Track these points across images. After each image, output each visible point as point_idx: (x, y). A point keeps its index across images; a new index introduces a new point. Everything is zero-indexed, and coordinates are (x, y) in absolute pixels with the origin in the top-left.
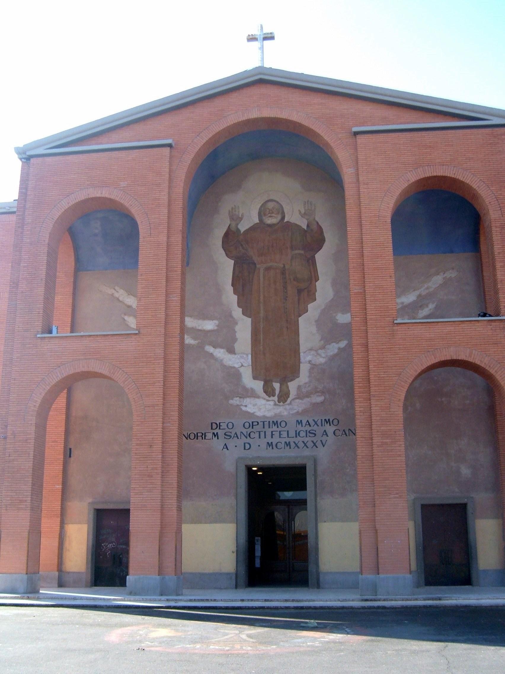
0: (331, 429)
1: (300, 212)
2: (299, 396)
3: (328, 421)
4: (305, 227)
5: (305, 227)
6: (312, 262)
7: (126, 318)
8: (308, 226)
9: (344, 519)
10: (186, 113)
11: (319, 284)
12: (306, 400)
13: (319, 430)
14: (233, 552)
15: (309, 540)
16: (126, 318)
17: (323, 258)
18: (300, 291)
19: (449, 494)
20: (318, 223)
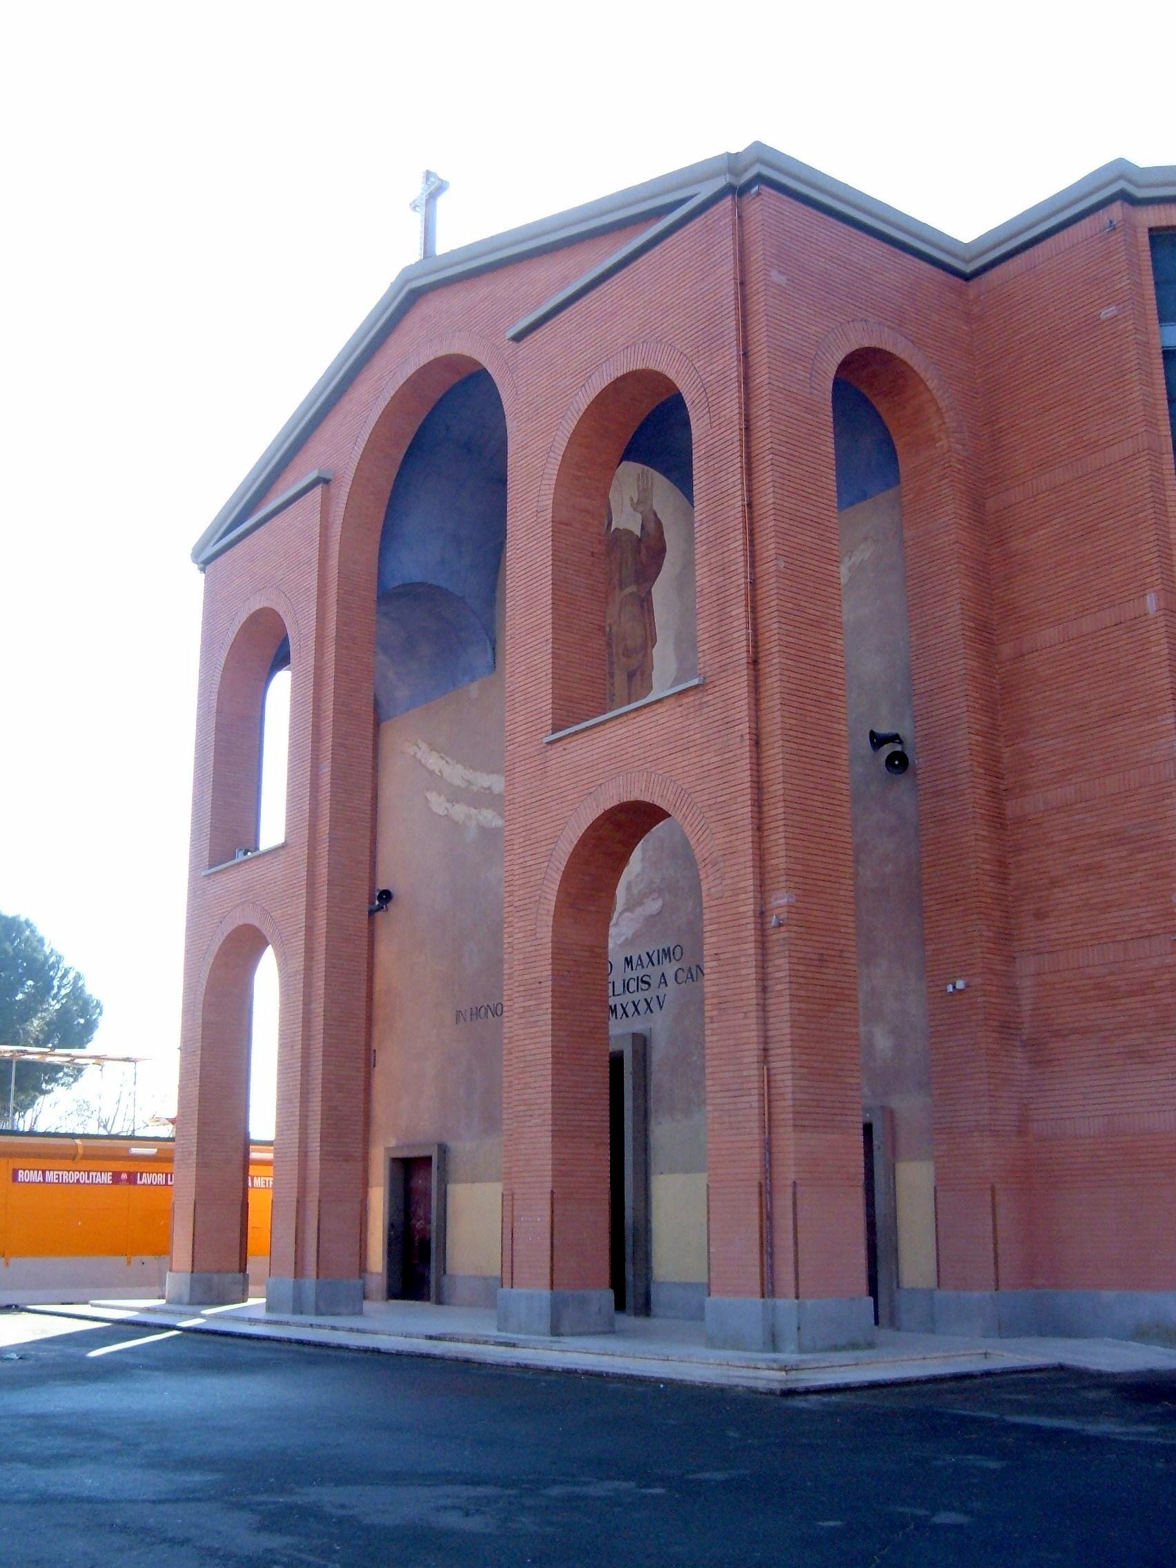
0: (670, 968)
1: (632, 499)
2: (628, 909)
3: (667, 953)
4: (638, 532)
5: (638, 532)
6: (645, 603)
7: (428, 795)
8: (643, 528)
9: (688, 1169)
10: (482, 289)
11: (656, 651)
12: (639, 910)
13: (654, 973)
14: (414, 207)
15: (632, 1317)
16: (428, 795)
17: (661, 591)
18: (631, 676)
19: (867, 1121)
20: (655, 515)
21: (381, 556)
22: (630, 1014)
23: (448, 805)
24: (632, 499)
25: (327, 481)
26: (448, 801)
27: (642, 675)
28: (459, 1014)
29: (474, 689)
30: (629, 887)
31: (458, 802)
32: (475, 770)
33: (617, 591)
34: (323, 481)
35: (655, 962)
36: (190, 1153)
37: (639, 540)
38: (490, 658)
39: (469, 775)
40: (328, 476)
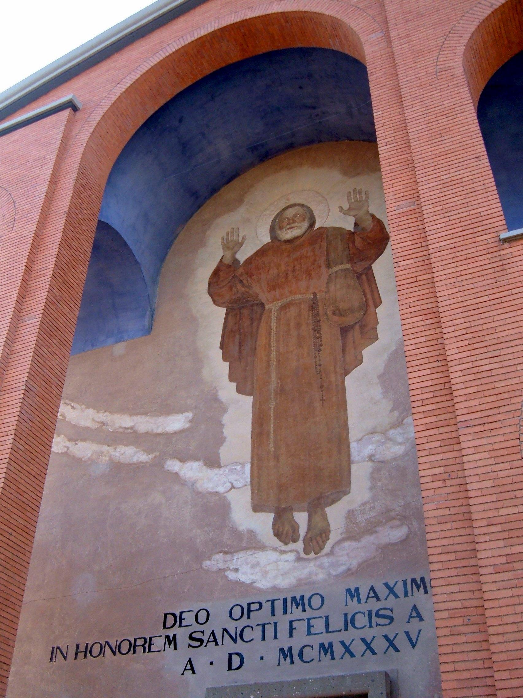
5: (352, 229)
17: (382, 268)
21: (110, 175)
22: (358, 654)
23: (68, 444)
24: (341, 208)
25: (75, 109)
26: (69, 440)
27: (362, 327)
28: (55, 652)
29: (119, 349)
30: (350, 515)
31: (84, 440)
32: (111, 412)
33: (324, 269)
34: (71, 106)
35: (401, 593)
36: (158, 428)
37: (352, 234)
38: (147, 323)
39: (102, 417)
40: (80, 105)
